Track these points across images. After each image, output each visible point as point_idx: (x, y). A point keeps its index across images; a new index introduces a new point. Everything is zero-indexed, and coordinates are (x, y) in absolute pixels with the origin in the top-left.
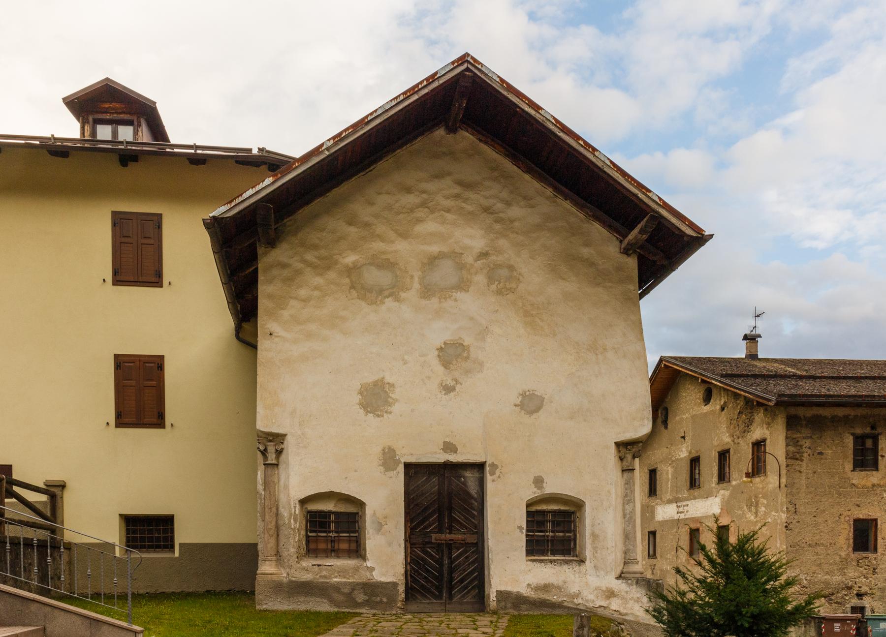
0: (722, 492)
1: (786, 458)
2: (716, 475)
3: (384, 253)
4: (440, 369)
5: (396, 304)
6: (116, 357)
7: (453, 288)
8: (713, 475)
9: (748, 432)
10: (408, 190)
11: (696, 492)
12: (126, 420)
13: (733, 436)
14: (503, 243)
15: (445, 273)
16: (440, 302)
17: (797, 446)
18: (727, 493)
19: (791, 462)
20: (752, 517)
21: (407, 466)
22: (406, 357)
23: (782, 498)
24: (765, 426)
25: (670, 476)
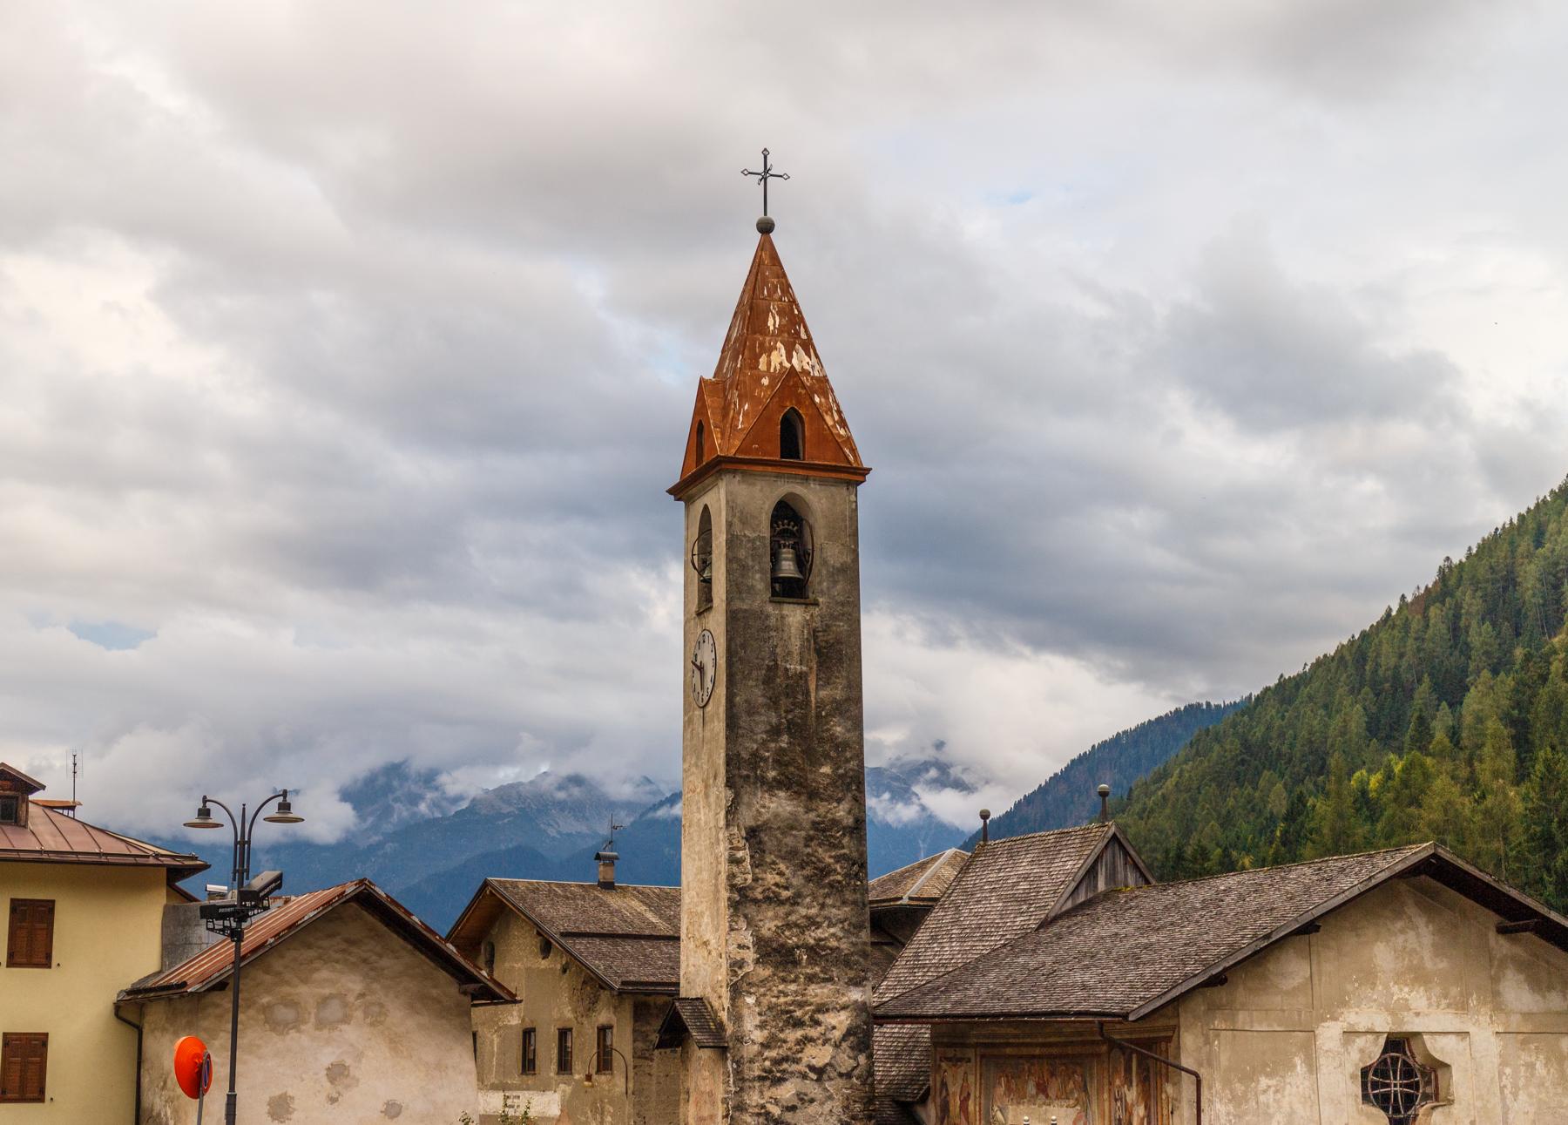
0: (562, 1086)
1: (634, 1057)
2: (555, 1061)
5: (298, 1034)
7: (338, 1022)
8: (551, 1060)
10: (309, 947)
11: (530, 1080)
14: (376, 986)
15: (334, 1010)
16: (330, 1033)
17: (647, 1041)
18: (568, 1089)
19: (640, 1062)
22: (304, 1076)
24: (611, 1008)
25: (495, 1049)
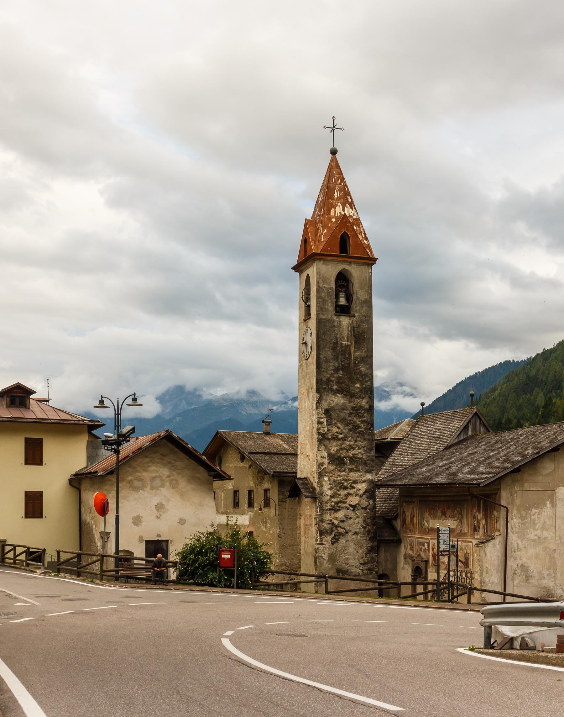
0: (250, 513)
1: (278, 501)
3: (139, 476)
4: (156, 511)
6: (26, 492)
9: (262, 483)
10: (147, 457)
11: (237, 510)
12: (29, 516)
13: (255, 484)
14: (174, 473)
15: (158, 482)
18: (252, 514)
19: (281, 503)
20: (264, 529)
21: (146, 541)
22: (146, 508)
23: (276, 521)
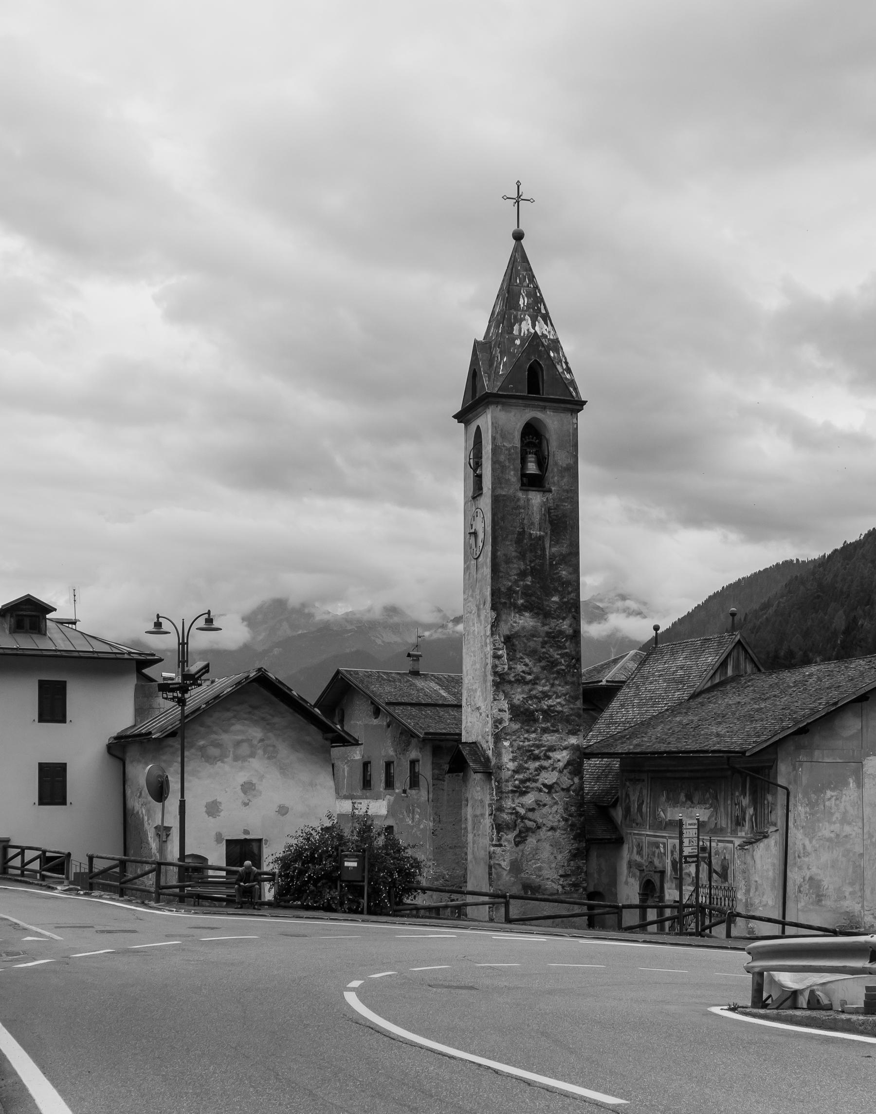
0: (388, 797)
3: (216, 740)
4: (242, 795)
6: (40, 764)
11: (368, 793)
14: (270, 734)
15: (245, 749)
18: (392, 798)
20: (410, 822)
21: (227, 841)
23: (429, 810)
